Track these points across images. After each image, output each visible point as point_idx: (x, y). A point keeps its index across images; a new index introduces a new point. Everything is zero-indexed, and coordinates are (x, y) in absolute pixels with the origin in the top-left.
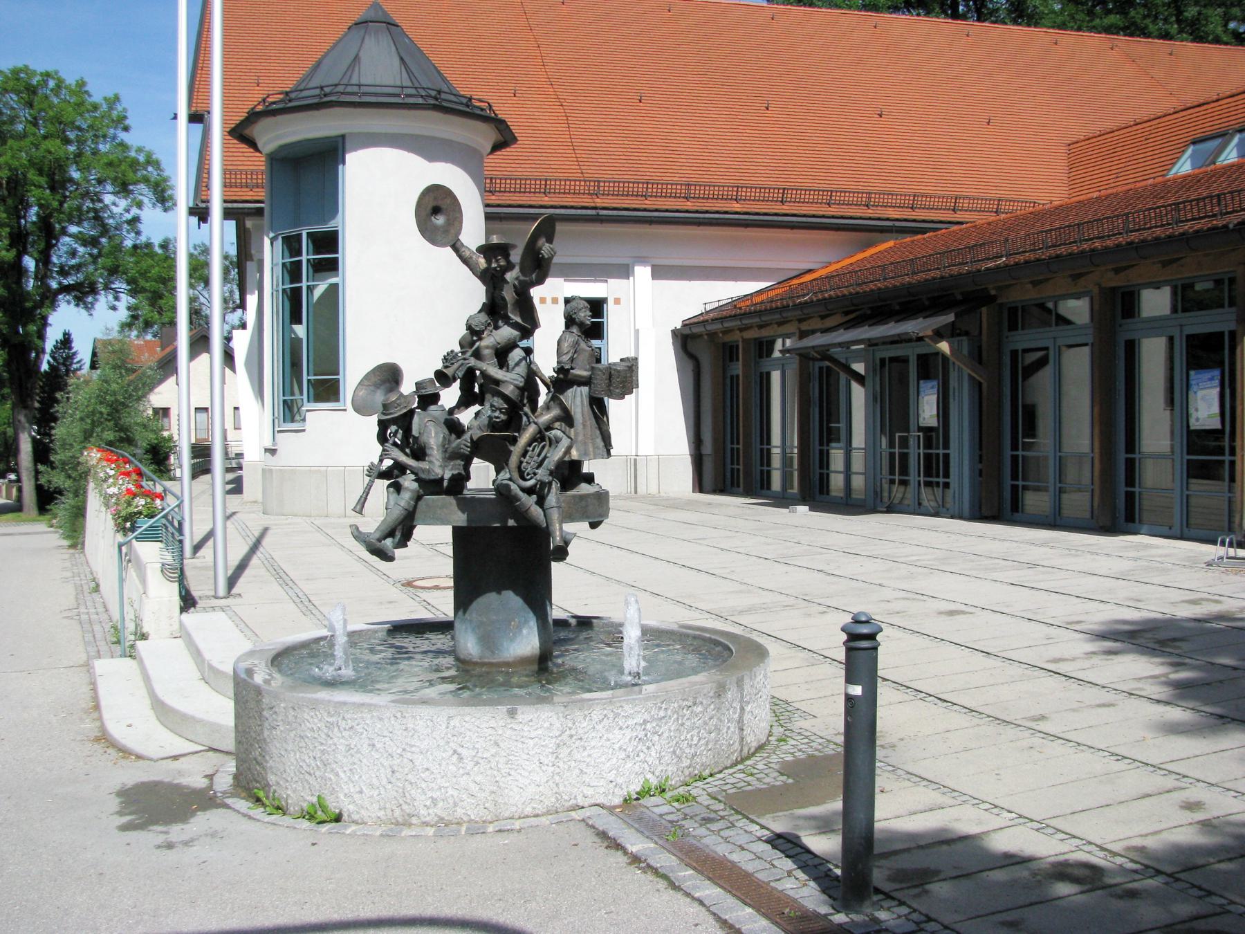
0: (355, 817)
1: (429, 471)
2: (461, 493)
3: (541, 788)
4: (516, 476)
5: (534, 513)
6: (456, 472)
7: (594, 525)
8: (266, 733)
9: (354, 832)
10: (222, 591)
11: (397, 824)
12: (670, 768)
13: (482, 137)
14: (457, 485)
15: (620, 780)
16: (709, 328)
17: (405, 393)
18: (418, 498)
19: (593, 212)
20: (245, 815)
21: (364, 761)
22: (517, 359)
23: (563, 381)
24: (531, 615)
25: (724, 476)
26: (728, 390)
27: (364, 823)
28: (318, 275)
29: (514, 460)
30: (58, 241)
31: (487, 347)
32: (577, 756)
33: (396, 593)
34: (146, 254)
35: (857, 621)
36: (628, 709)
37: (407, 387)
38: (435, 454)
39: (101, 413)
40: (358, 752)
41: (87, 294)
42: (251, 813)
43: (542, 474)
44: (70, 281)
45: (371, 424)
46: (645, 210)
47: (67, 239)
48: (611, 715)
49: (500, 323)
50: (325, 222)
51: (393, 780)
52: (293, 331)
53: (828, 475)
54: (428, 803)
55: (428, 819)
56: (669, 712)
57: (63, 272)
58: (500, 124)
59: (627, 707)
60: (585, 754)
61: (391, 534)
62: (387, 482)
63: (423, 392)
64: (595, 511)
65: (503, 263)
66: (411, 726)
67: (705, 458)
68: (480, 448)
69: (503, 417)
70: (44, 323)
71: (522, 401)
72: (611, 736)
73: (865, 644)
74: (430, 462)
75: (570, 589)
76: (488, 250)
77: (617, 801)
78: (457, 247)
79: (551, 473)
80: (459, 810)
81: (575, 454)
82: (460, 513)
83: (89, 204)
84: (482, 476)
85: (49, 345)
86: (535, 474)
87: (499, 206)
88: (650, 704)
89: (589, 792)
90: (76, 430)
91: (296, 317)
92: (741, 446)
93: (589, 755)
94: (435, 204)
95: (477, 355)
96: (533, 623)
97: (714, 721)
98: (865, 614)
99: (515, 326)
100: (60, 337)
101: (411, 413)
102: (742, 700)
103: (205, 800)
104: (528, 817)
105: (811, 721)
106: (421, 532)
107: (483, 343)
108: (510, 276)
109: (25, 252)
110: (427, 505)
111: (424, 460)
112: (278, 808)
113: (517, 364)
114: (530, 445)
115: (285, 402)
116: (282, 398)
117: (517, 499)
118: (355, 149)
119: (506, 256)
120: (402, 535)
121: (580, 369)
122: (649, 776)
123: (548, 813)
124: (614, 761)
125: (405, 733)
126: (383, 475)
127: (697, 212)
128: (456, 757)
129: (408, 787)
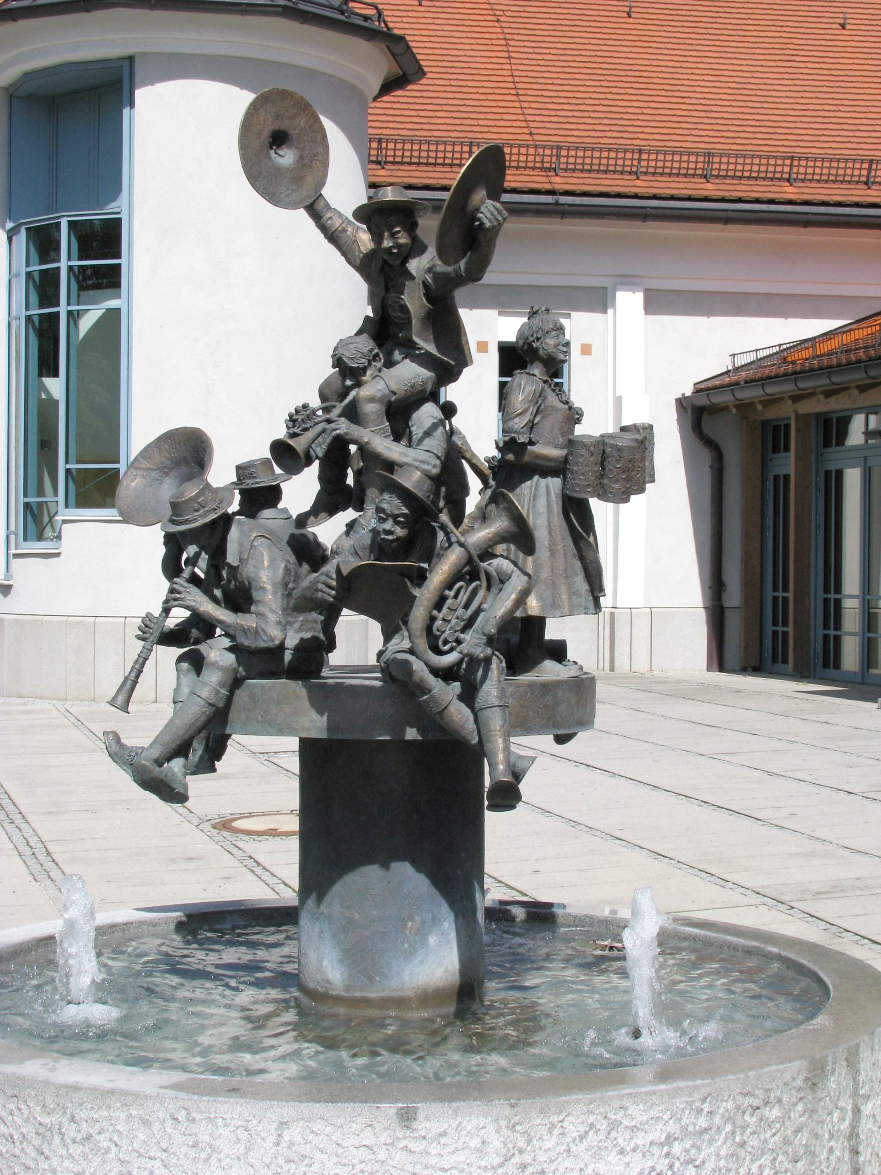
1: (256, 632)
2: (317, 674)
4: (422, 644)
5: (457, 718)
6: (308, 635)
7: (561, 740)
13: (367, 66)
14: (309, 661)
16: (740, 395)
17: (215, 485)
18: (236, 683)
22: (428, 424)
23: (513, 466)
29: (418, 615)
31: (372, 400)
33: (201, 842)
36: (637, 1112)
37: (221, 474)
43: (473, 643)
45: (151, 541)
46: (636, 196)
48: (603, 1126)
49: (397, 355)
50: (101, 205)
52: (43, 388)
56: (717, 1120)
58: (395, 44)
59: (633, 1109)
61: (182, 750)
62: (176, 652)
63: (250, 483)
64: (567, 711)
65: (403, 239)
66: (205, 1138)
67: (729, 614)
68: (354, 590)
69: (400, 532)
71: (435, 502)
74: (259, 615)
75: (515, 855)
76: (374, 215)
78: (316, 211)
79: (490, 641)
81: (533, 606)
82: (314, 715)
84: (358, 642)
86: (459, 642)
88: (679, 1103)
91: (47, 364)
92: (790, 595)
94: (276, 126)
95: (353, 413)
96: (448, 925)
97: (804, 1137)
99: (426, 360)
101: (226, 520)
102: (855, 1094)
106: (241, 749)
107: (364, 392)
108: (415, 266)
110: (252, 696)
111: (248, 611)
113: (428, 433)
114: (450, 587)
115: (27, 505)
116: (22, 500)
117: (422, 688)
118: (151, 81)
119: (411, 227)
120: (207, 749)
121: (548, 443)
125: (192, 1153)
126: (170, 638)
127: (723, 200)
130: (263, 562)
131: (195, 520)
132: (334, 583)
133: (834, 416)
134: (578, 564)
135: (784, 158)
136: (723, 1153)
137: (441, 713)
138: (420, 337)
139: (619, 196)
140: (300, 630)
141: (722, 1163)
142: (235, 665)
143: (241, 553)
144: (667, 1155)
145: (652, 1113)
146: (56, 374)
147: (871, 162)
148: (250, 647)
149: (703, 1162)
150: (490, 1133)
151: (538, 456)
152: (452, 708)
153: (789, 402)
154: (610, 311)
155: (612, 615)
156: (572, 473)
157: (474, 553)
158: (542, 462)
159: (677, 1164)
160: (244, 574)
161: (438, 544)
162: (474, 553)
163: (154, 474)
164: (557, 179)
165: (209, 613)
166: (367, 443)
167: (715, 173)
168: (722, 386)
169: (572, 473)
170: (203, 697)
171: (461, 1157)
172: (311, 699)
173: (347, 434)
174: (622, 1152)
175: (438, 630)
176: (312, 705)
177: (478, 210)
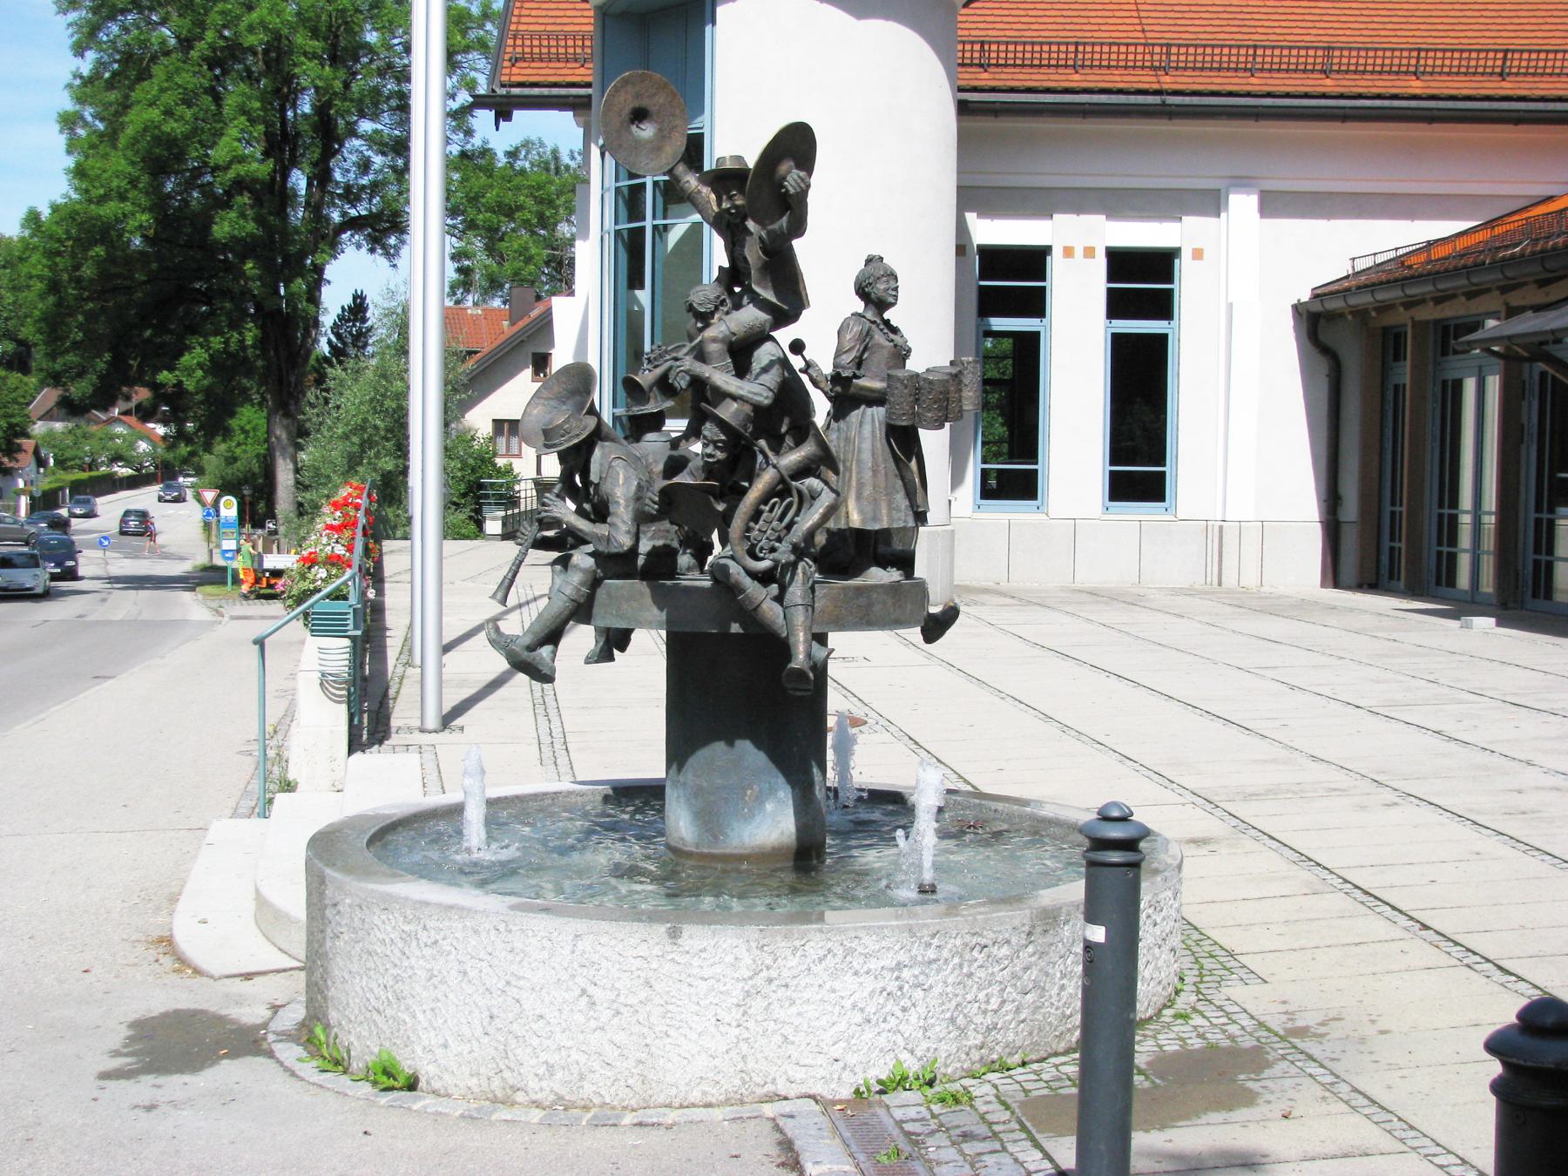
0: (436, 1085)
3: (717, 1062)
4: (741, 551)
6: (660, 543)
8: (329, 944)
9: (425, 1107)
10: (432, 721)
11: (495, 1100)
12: (943, 1046)
15: (852, 1059)
16: (1353, 301)
18: (595, 583)
19: (1156, 99)
20: (287, 1069)
21: (451, 996)
22: (765, 362)
24: (781, 780)
25: (1378, 561)
26: (1387, 406)
27: (448, 1096)
28: (673, 208)
30: (342, 145)
31: (714, 340)
32: (780, 1014)
34: (480, 168)
35: (1105, 818)
36: (870, 943)
38: (623, 514)
39: (376, 427)
40: (443, 982)
41: (386, 232)
42: (297, 1067)
43: (784, 554)
44: (362, 210)
46: (1248, 95)
47: (356, 143)
48: (840, 951)
51: (491, 1030)
53: (1550, 567)
54: (540, 1072)
55: (539, 1096)
56: (945, 953)
57: (351, 195)
59: (866, 940)
60: (794, 1010)
66: (518, 945)
69: (720, 455)
70: (317, 279)
72: (837, 985)
73: (1115, 857)
77: (846, 1093)
80: (586, 1084)
82: (655, 610)
83: (391, 86)
85: (328, 320)
87: (993, 90)
89: (799, 1074)
90: (337, 453)
92: (1404, 509)
93: (799, 1014)
94: (636, 104)
98: (1116, 804)
99: (763, 305)
100: (348, 301)
103: (248, 1042)
104: (694, 1105)
105: (1255, 988)
107: (709, 333)
109: (295, 162)
112: (337, 1063)
113: (765, 370)
122: (904, 1056)
123: (727, 1102)
124: (842, 1026)
125: (510, 957)
127: (1342, 96)
128: (584, 1000)
129: (513, 1043)
133: (1452, 323)
134: (900, 482)
135: (1410, 50)
136: (950, 980)
137: (755, 609)
138: (758, 284)
139: (1231, 94)
140: (652, 538)
141: (949, 989)
144: (897, 978)
145: (884, 944)
146: (642, 287)
147: (1506, 52)
149: (931, 987)
150: (742, 951)
152: (764, 606)
153: (1401, 309)
154: (1223, 215)
155: (1221, 528)
159: (906, 987)
162: (785, 474)
163: (552, 403)
164: (1167, 79)
167: (1335, 68)
168: (1338, 292)
171: (718, 969)
172: (653, 597)
174: (856, 973)
177: (784, 179)
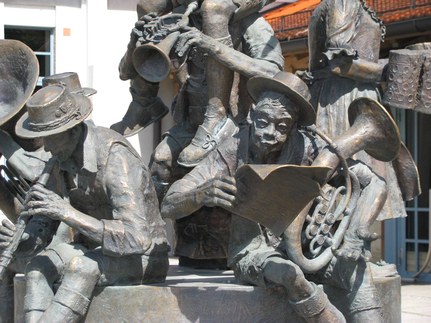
18: (97, 289)
69: (280, 137)
111: (110, 217)
130: (122, 167)
131: (56, 126)
132: (233, 188)
142: (98, 272)
143: (99, 159)
148: (118, 254)
151: (361, 69)
152: (327, 311)
154: (83, 6)
156: (396, 85)
157: (345, 158)
158: (363, 75)
160: (104, 180)
161: (306, 150)
165: (73, 220)
166: (219, 52)
169: (396, 85)
170: (69, 305)
173: (202, 43)
175: (310, 234)
176: (183, 312)
